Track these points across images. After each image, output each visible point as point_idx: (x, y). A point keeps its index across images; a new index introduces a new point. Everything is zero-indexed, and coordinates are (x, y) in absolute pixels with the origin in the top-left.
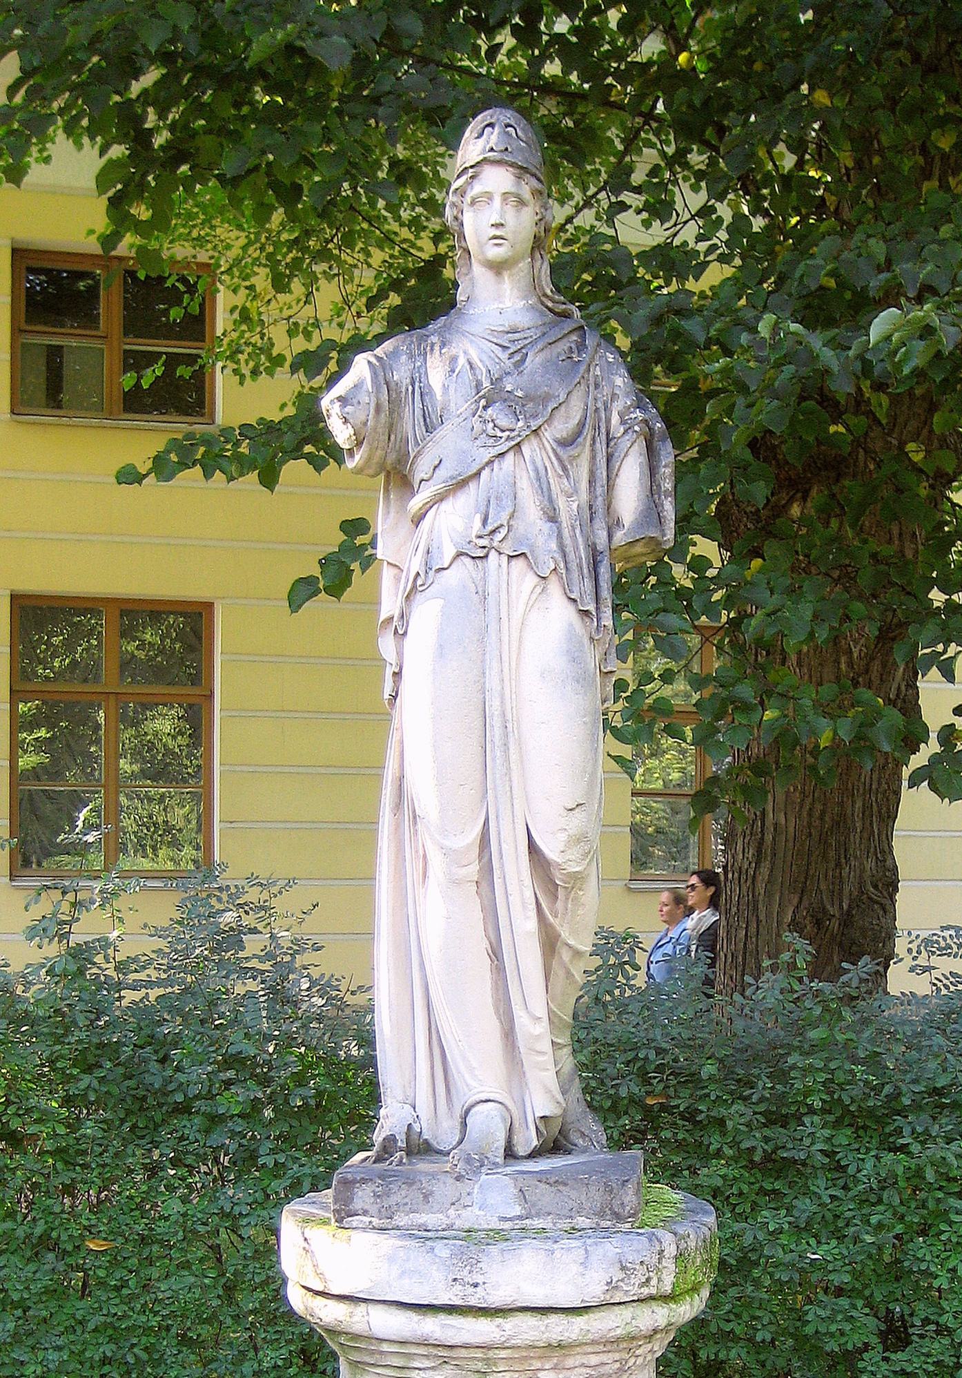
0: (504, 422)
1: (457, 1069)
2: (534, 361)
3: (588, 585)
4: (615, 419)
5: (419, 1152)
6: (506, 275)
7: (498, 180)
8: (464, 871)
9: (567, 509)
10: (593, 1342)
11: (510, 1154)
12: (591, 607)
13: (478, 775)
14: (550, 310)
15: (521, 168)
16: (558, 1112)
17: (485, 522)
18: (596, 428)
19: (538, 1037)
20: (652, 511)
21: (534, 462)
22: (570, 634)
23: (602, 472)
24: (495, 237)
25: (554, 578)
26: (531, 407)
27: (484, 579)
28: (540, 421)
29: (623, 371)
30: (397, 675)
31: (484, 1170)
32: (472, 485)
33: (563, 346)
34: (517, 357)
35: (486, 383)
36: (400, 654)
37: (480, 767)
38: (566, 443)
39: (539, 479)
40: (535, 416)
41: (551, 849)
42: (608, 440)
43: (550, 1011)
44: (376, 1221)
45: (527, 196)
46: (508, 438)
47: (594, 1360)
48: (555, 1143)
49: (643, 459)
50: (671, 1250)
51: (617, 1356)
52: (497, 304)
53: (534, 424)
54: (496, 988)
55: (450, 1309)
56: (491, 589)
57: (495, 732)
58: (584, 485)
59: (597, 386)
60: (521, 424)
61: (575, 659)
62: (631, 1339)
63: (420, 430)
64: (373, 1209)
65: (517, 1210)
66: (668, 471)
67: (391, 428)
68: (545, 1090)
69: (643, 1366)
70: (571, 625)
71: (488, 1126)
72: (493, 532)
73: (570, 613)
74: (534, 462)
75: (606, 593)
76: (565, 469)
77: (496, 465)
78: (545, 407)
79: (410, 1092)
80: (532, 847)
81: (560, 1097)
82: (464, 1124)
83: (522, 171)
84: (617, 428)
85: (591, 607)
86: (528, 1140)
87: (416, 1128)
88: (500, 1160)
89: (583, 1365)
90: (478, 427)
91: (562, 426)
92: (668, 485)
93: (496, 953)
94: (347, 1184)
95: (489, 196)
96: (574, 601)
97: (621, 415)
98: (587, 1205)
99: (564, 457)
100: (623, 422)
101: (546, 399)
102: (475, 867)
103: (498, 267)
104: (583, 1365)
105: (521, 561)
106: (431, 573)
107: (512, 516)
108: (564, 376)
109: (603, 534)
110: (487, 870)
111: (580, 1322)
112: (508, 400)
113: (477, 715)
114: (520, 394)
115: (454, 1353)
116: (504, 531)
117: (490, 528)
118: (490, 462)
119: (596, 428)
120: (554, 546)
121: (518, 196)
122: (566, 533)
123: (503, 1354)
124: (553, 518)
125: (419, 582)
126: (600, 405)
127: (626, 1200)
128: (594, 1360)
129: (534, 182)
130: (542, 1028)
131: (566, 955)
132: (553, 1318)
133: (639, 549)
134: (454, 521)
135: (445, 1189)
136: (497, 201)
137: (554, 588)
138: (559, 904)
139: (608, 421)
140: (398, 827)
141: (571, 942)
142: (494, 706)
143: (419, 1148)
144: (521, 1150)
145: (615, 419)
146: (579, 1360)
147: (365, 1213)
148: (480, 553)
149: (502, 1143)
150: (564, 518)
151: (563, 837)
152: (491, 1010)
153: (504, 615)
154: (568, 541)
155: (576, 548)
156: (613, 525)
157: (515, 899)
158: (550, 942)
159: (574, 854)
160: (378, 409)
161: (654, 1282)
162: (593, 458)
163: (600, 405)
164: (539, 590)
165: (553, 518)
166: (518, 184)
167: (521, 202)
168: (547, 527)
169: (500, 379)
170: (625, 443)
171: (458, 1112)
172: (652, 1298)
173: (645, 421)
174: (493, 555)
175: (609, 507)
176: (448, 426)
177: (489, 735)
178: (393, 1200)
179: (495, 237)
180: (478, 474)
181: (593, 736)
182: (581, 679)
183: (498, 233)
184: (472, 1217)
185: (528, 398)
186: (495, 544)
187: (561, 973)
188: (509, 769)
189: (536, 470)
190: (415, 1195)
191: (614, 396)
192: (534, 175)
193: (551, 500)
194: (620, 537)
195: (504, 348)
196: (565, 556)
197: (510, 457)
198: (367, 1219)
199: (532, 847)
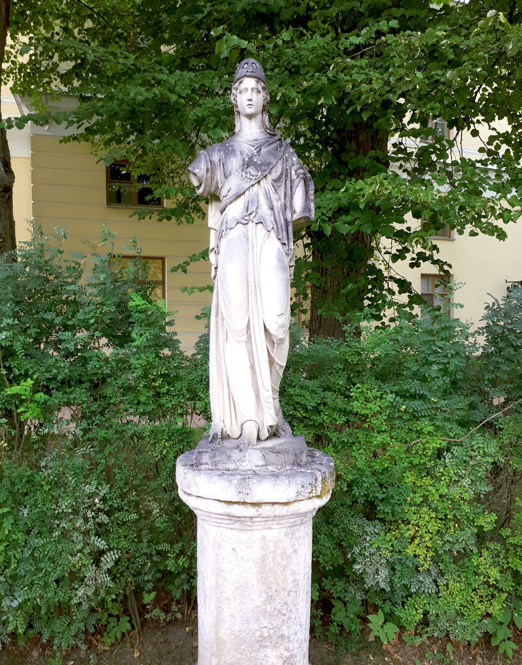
0: (254, 173)
1: (218, 292)
2: (264, 150)
3: (285, 233)
4: (293, 173)
5: (226, 438)
6: (253, 120)
7: (249, 83)
8: (243, 338)
9: (278, 205)
10: (292, 515)
11: (259, 439)
12: (286, 242)
13: (246, 304)
14: (269, 134)
15: (259, 78)
16: (275, 423)
17: (247, 210)
18: (286, 176)
19: (268, 398)
20: (306, 208)
21: (265, 188)
22: (279, 252)
23: (289, 192)
24: (249, 105)
25: (272, 231)
26: (264, 168)
27: (247, 232)
28: (267, 172)
29: (296, 155)
30: (216, 268)
31: (250, 447)
32: (242, 197)
33: (274, 145)
34: (258, 149)
35: (247, 159)
36: (217, 261)
37: (246, 301)
38: (275, 181)
39: (266, 194)
40: (265, 171)
41: (272, 330)
42: (291, 181)
43: (273, 388)
44: (210, 467)
45: (261, 89)
46: (255, 179)
47: (292, 520)
48: (274, 434)
49: (303, 188)
50: (320, 479)
51: (300, 518)
52: (250, 131)
53: (265, 174)
54: (253, 380)
55: (238, 503)
56: (250, 235)
57: (252, 288)
58: (283, 197)
59: (287, 161)
60: (260, 174)
61: (280, 260)
62: (305, 514)
63: (223, 178)
64: (209, 463)
65: (262, 463)
66: (312, 192)
67: (212, 178)
68: (270, 415)
69: (307, 521)
70: (279, 248)
71: (251, 430)
72: (250, 214)
73: (278, 244)
74: (265, 188)
75: (291, 236)
76: (276, 190)
77: (251, 189)
78: (268, 167)
79: (222, 417)
80: (266, 329)
81: (276, 418)
82: (242, 429)
83: (259, 80)
84: (294, 176)
85: (286, 242)
86: (265, 434)
87: (225, 430)
88: (255, 443)
89: (287, 523)
90: (244, 175)
91: (275, 174)
92: (312, 197)
93: (253, 367)
94: (200, 453)
95: (247, 89)
96: (280, 239)
97: (296, 171)
98: (288, 461)
99: (276, 186)
100: (296, 174)
101: (269, 164)
102: (245, 336)
103: (250, 117)
104: (287, 523)
105: (260, 225)
106: (228, 230)
107: (257, 208)
108: (275, 156)
109: (290, 215)
110: (249, 338)
111: (286, 508)
112: (255, 164)
113: (245, 282)
114: (259, 162)
115: (240, 519)
116: (254, 214)
117: (249, 212)
118: (249, 188)
119: (286, 176)
120: (272, 218)
121: (257, 89)
122: (276, 214)
123: (258, 519)
124: (272, 209)
125: (223, 233)
126: (288, 167)
127: (303, 459)
128: (292, 520)
129: (263, 84)
130: (270, 394)
131: (277, 367)
132: (276, 506)
133: (302, 221)
134: (235, 210)
135: (236, 454)
136: (250, 90)
137: (273, 235)
138: (275, 349)
139: (291, 174)
140: (217, 323)
141: (279, 363)
142: (251, 279)
143: (225, 437)
144: (263, 438)
145: (293, 173)
146: (286, 521)
147: (206, 464)
148: (245, 222)
149: (256, 436)
150: (275, 209)
151: (277, 325)
152: (251, 388)
153: (254, 245)
154: (277, 218)
155: (280, 220)
156: (293, 212)
157: (259, 349)
158: (272, 362)
159: (281, 331)
160: (207, 171)
161: (314, 491)
162: (286, 187)
163: (288, 167)
164: (267, 235)
165: (272, 209)
166: (257, 85)
167: (259, 92)
168: (269, 212)
169: (252, 158)
170: (297, 181)
171: (239, 424)
172: (313, 497)
173: (304, 174)
174: (250, 222)
175: (291, 205)
176: (233, 176)
177: (251, 288)
178: (217, 458)
179: (249, 105)
180: (244, 192)
181: (287, 289)
182: (283, 268)
183: (250, 103)
184: (246, 465)
185: (262, 165)
186: (251, 218)
187: (276, 374)
188: (257, 301)
189: (266, 191)
190: (224, 458)
191: (293, 165)
192: (263, 81)
193: (271, 202)
194: (295, 217)
195: (253, 146)
196: (276, 222)
197: (256, 186)
198: (207, 466)
199: (266, 329)
